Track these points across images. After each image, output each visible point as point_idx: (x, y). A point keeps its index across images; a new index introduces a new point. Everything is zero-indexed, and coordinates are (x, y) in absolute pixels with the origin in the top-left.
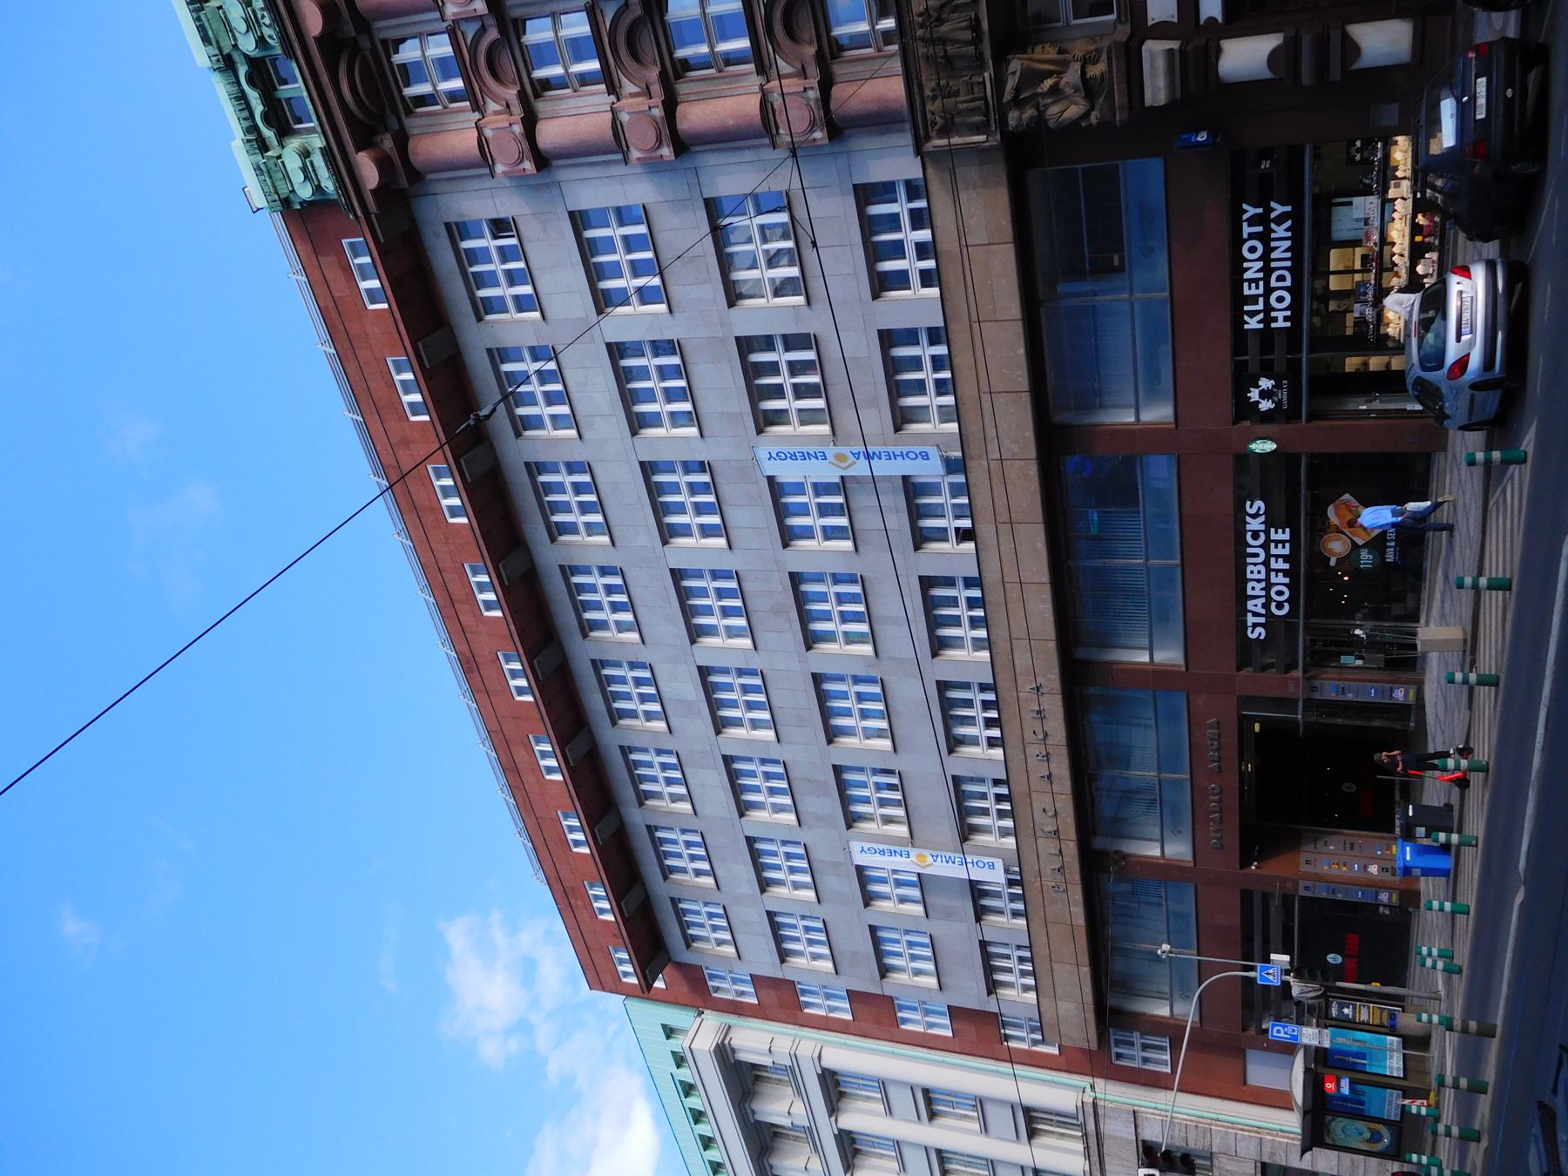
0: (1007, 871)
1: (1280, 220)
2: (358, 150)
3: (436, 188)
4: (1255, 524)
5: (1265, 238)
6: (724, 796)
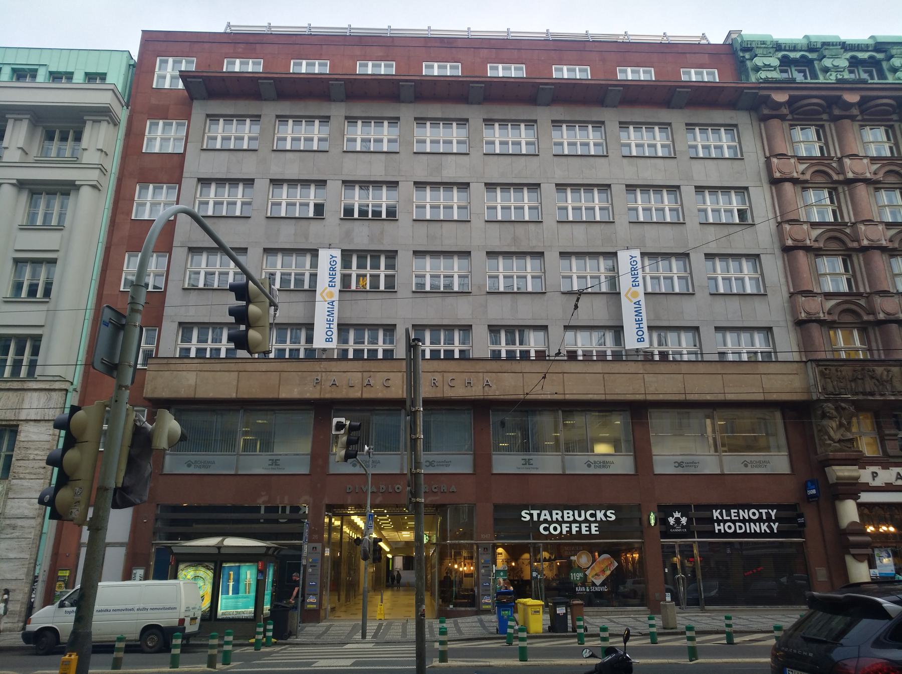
0: (324, 350)
1: (770, 527)
2: (790, 96)
3: (756, 124)
4: (600, 515)
5: (760, 520)
6: (361, 174)
